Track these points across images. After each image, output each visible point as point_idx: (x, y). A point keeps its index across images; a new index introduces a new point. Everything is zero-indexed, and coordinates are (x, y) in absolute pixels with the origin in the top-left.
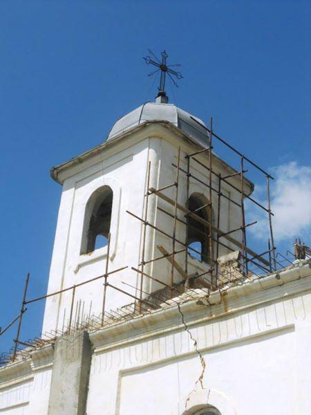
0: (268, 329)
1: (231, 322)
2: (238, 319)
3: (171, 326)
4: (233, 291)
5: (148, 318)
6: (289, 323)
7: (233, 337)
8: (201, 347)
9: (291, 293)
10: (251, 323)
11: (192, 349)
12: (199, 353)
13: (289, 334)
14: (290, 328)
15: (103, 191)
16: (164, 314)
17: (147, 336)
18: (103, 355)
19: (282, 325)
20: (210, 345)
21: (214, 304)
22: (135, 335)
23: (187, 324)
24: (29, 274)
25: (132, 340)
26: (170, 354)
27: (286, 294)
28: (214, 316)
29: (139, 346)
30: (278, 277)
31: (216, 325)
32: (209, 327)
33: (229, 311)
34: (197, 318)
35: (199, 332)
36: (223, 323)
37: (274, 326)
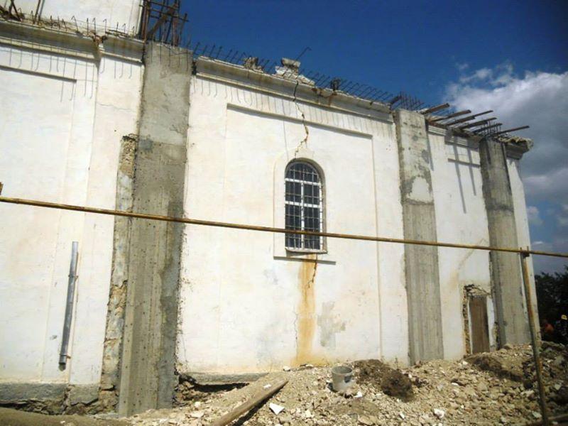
0: (355, 130)
1: (329, 113)
2: (335, 114)
3: (284, 92)
4: (341, 96)
5: (266, 77)
6: (370, 133)
7: (331, 124)
8: (307, 119)
9: (372, 116)
10: (344, 121)
11: (300, 117)
12: (303, 122)
13: (259, 117)
14: (369, 137)
15: (482, 74)
16: (283, 82)
17: (258, 89)
18: (206, 83)
19: (365, 132)
20: (314, 121)
21: (322, 96)
22: (247, 83)
23: (297, 98)
24: (527, 127)
25: (242, 85)
26: (280, 112)
27: (369, 115)
28: (319, 104)
29: (248, 93)
30: (371, 104)
31: (318, 110)
32: (312, 109)
33: (331, 106)
34: (307, 98)
35: (306, 108)
36: (324, 112)
37: (360, 130)
